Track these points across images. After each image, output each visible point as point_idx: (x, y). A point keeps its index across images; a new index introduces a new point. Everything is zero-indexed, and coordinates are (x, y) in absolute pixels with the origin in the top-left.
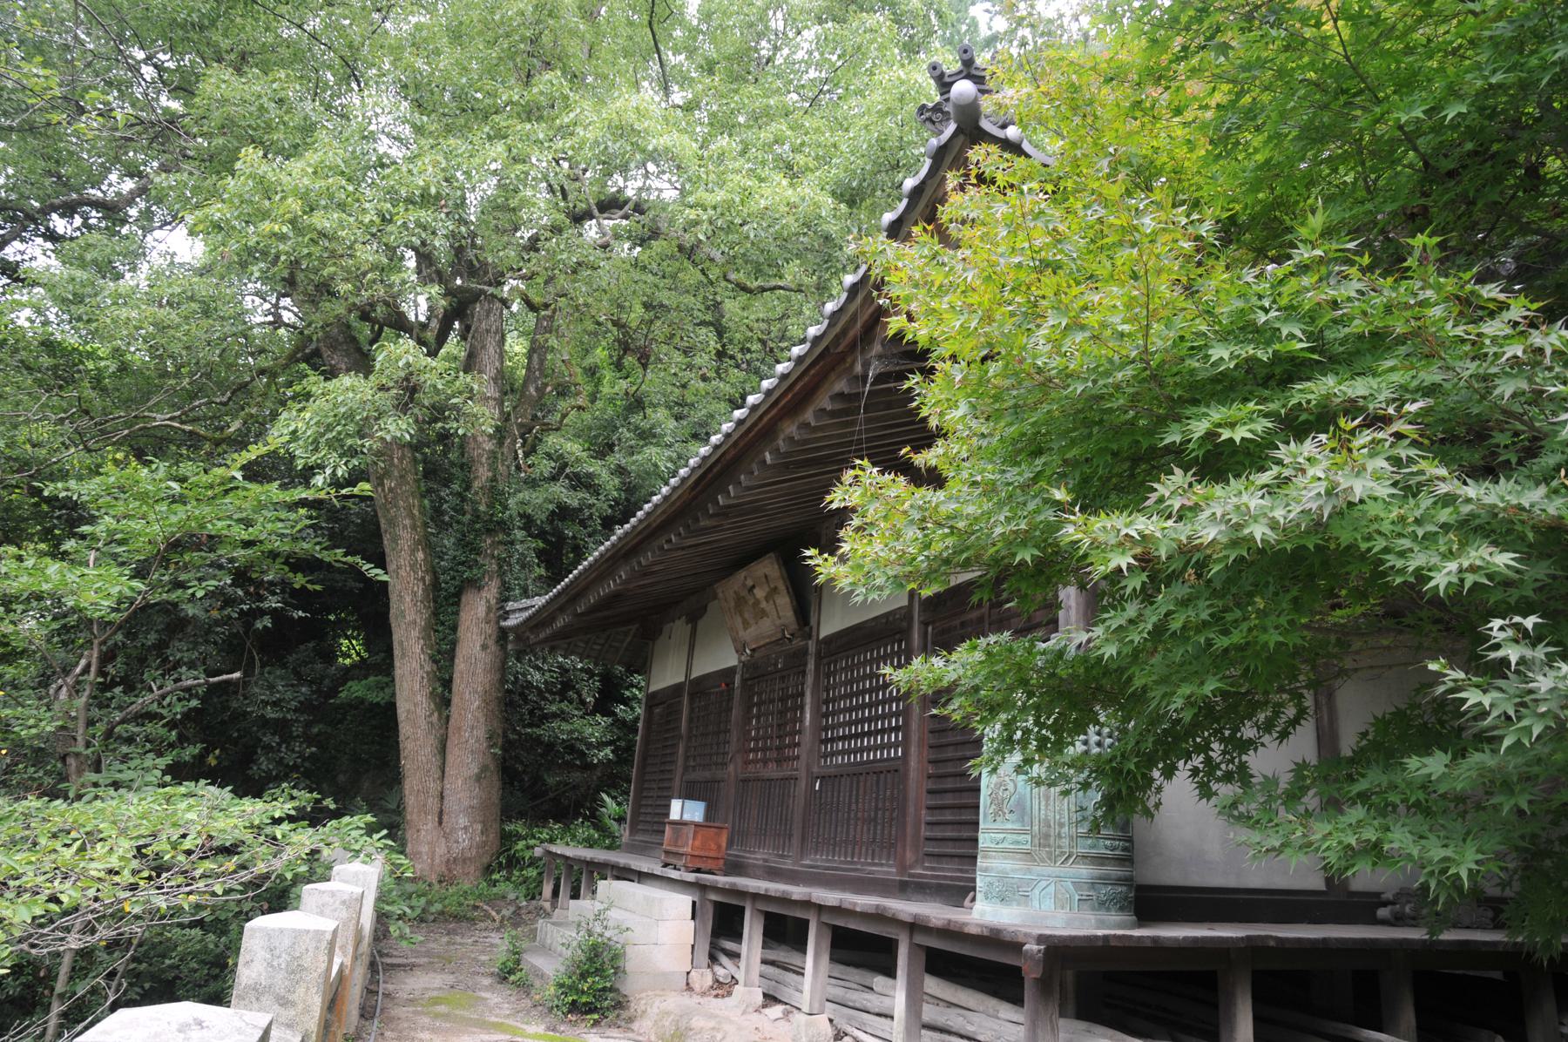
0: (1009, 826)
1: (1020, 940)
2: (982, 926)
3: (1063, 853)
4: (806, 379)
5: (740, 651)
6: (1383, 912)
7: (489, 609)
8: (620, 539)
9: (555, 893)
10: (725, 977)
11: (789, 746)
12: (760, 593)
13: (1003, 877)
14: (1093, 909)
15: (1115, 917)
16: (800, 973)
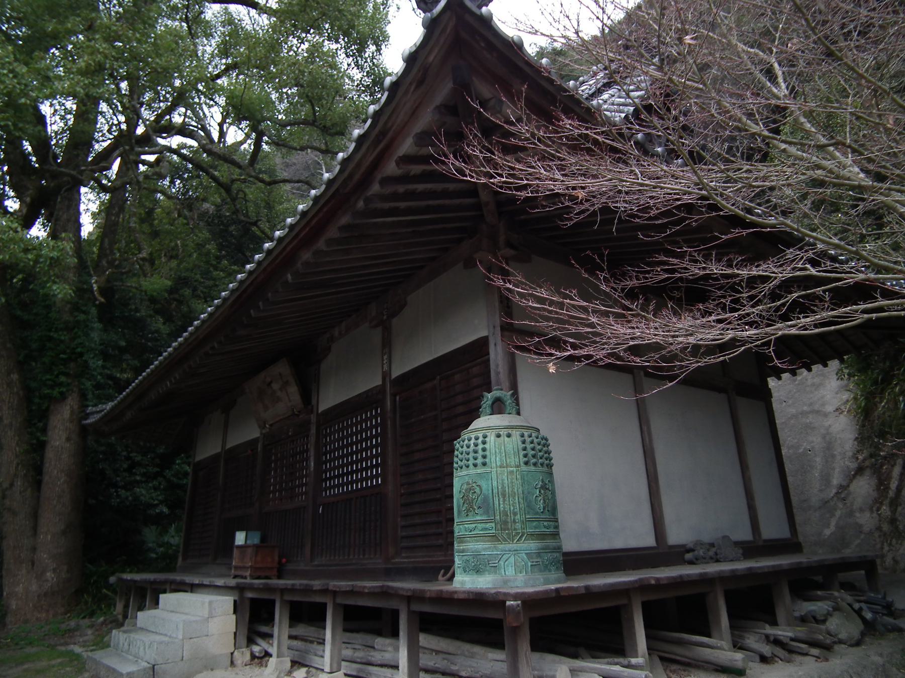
0: (478, 518)
1: (501, 598)
2: (464, 592)
3: (518, 534)
4: (321, 215)
5: (262, 426)
6: (688, 556)
7: (72, 412)
8: (175, 349)
9: (126, 606)
10: (260, 652)
11: (299, 486)
12: (276, 386)
13: (476, 555)
14: (541, 571)
15: (539, 577)
16: (322, 642)
